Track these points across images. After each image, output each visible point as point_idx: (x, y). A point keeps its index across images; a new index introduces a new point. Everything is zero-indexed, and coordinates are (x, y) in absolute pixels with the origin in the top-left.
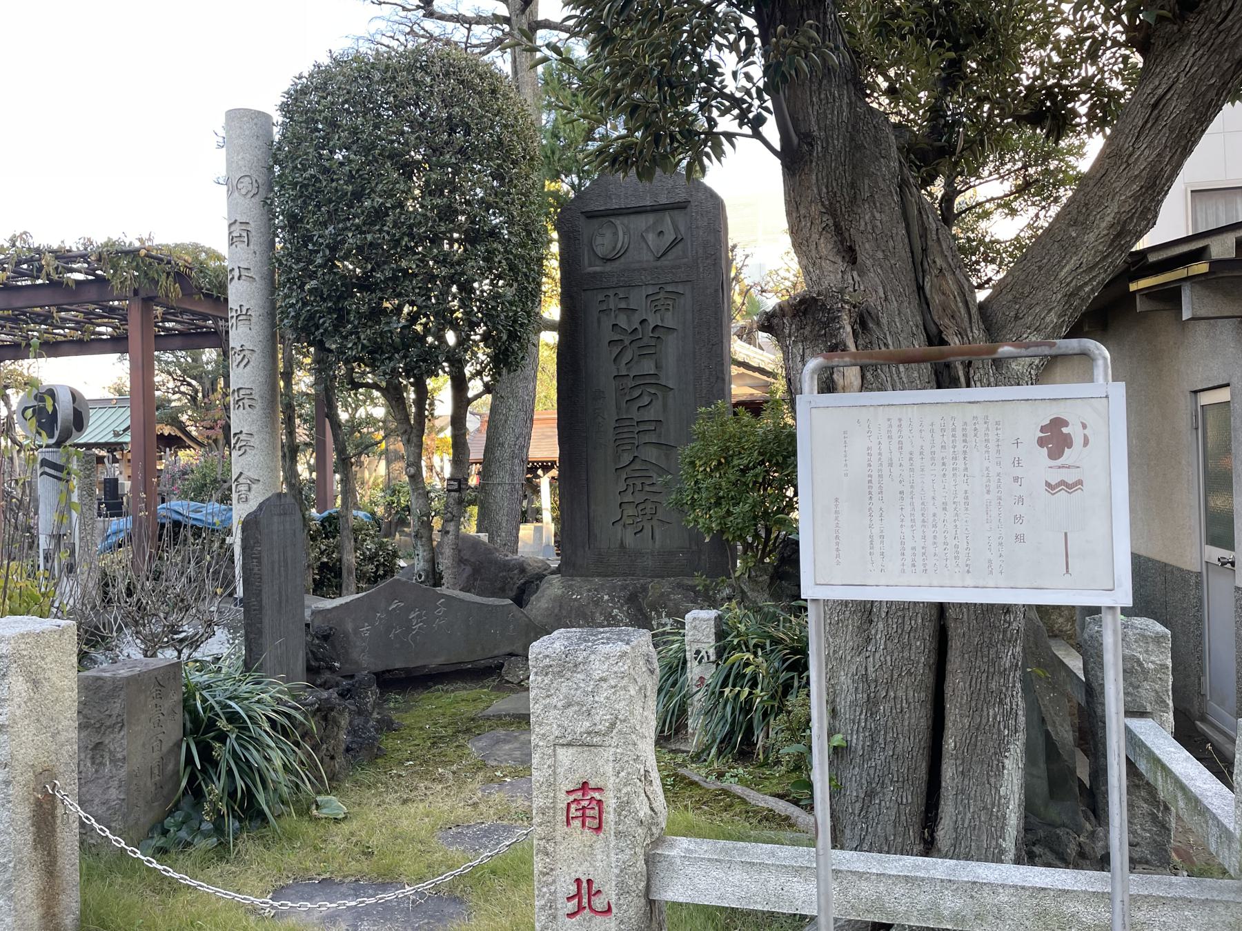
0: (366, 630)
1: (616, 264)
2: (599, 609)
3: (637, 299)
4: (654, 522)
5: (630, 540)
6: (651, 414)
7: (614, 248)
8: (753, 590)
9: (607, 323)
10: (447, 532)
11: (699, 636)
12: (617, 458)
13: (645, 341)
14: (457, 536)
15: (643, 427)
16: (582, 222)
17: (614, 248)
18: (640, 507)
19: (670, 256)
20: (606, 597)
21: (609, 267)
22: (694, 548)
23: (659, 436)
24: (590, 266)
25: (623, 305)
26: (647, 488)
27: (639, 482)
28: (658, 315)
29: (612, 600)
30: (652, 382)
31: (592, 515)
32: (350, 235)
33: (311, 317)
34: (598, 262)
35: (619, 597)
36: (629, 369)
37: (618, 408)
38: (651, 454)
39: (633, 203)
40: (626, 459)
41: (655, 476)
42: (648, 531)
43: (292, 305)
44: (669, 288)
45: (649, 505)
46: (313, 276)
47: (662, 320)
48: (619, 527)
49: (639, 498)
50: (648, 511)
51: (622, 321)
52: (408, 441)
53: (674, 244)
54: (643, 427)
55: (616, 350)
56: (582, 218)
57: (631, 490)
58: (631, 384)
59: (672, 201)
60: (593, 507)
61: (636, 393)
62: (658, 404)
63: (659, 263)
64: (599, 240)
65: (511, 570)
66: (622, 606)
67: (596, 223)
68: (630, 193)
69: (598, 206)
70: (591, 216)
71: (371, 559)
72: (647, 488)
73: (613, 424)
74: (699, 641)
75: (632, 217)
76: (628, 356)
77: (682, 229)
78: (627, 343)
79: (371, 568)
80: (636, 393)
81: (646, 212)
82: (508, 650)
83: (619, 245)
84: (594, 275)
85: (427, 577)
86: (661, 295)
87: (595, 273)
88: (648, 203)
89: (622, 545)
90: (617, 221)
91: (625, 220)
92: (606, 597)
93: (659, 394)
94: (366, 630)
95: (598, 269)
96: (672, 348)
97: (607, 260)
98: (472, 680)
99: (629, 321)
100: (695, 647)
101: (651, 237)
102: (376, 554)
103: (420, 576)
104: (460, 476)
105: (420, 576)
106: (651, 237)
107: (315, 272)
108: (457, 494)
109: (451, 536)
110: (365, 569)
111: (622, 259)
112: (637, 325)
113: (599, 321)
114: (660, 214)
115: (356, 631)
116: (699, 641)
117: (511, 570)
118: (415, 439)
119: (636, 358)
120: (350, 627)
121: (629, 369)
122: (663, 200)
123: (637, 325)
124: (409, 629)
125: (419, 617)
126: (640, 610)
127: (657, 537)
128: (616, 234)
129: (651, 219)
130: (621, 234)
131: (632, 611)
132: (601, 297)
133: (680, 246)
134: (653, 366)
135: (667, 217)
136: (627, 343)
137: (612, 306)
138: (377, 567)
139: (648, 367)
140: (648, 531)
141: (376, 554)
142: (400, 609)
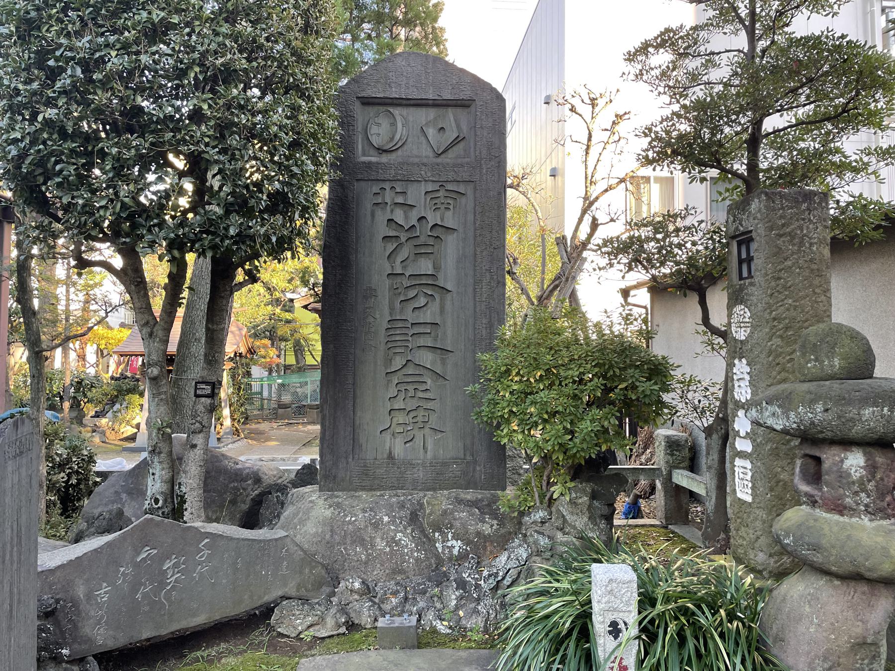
0: (104, 593)
1: (393, 156)
2: (380, 533)
3: (416, 194)
4: (427, 431)
5: (399, 450)
6: (427, 316)
7: (392, 139)
8: (572, 513)
9: (381, 217)
10: (194, 446)
11: (617, 603)
12: (389, 361)
13: (422, 240)
14: (206, 450)
15: (416, 330)
16: (357, 107)
17: (392, 139)
18: (412, 414)
19: (451, 154)
20: (386, 519)
21: (384, 159)
22: (469, 458)
23: (435, 340)
24: (364, 155)
25: (400, 200)
26: (421, 395)
27: (411, 388)
28: (438, 214)
29: (392, 522)
30: (431, 284)
31: (357, 423)
32: (114, 53)
33: (41, 162)
34: (372, 152)
35: (401, 518)
36: (404, 268)
37: (392, 309)
38: (427, 359)
39: (415, 94)
40: (398, 362)
41: (429, 382)
42: (419, 441)
43: (15, 141)
44: (450, 187)
45: (421, 413)
46: (50, 103)
47: (442, 220)
48: (387, 436)
49: (412, 404)
50: (420, 419)
51: (399, 216)
52: (151, 335)
53: (457, 141)
54: (416, 330)
55: (391, 247)
56: (358, 104)
57: (402, 395)
58: (406, 283)
59: (456, 97)
60: (359, 414)
61: (412, 293)
62: (435, 306)
63: (439, 160)
64: (374, 130)
65: (244, 480)
66: (405, 528)
67: (372, 110)
68: (411, 83)
69: (370, 92)
70: (367, 102)
71: (61, 466)
72: (421, 395)
73: (385, 325)
74: (615, 610)
75: (412, 109)
76: (404, 253)
77: (464, 127)
78: (403, 239)
79: (62, 477)
80: (412, 293)
81: (427, 105)
82: (280, 593)
83: (397, 137)
84: (369, 165)
85: (165, 501)
86: (441, 194)
87: (370, 163)
88: (431, 97)
89: (390, 456)
90: (396, 111)
91: (405, 111)
92: (386, 519)
93: (437, 296)
94: (104, 593)
95: (373, 159)
96: (451, 248)
97: (381, 151)
98: (235, 636)
99: (406, 218)
100: (610, 617)
101: (431, 132)
102: (69, 460)
103: (157, 501)
104: (214, 379)
105: (157, 501)
106: (431, 132)
107: (55, 99)
108: (208, 401)
109: (198, 452)
110: (55, 478)
111: (400, 152)
112: (414, 222)
113: (373, 215)
114: (441, 111)
115: (89, 596)
116: (615, 610)
117: (244, 480)
118: (160, 333)
119: (412, 257)
120: (81, 591)
121: (404, 268)
122: (447, 95)
123: (414, 222)
124: (162, 584)
125: (176, 566)
126: (423, 531)
127: (430, 447)
128: (393, 124)
129: (432, 113)
130: (399, 125)
131: (416, 534)
132: (376, 189)
133: (461, 145)
134: (430, 266)
135: (450, 113)
136: (403, 239)
137: (388, 200)
138: (69, 475)
139: (425, 266)
140: (419, 441)
141: (69, 460)
142: (152, 559)
